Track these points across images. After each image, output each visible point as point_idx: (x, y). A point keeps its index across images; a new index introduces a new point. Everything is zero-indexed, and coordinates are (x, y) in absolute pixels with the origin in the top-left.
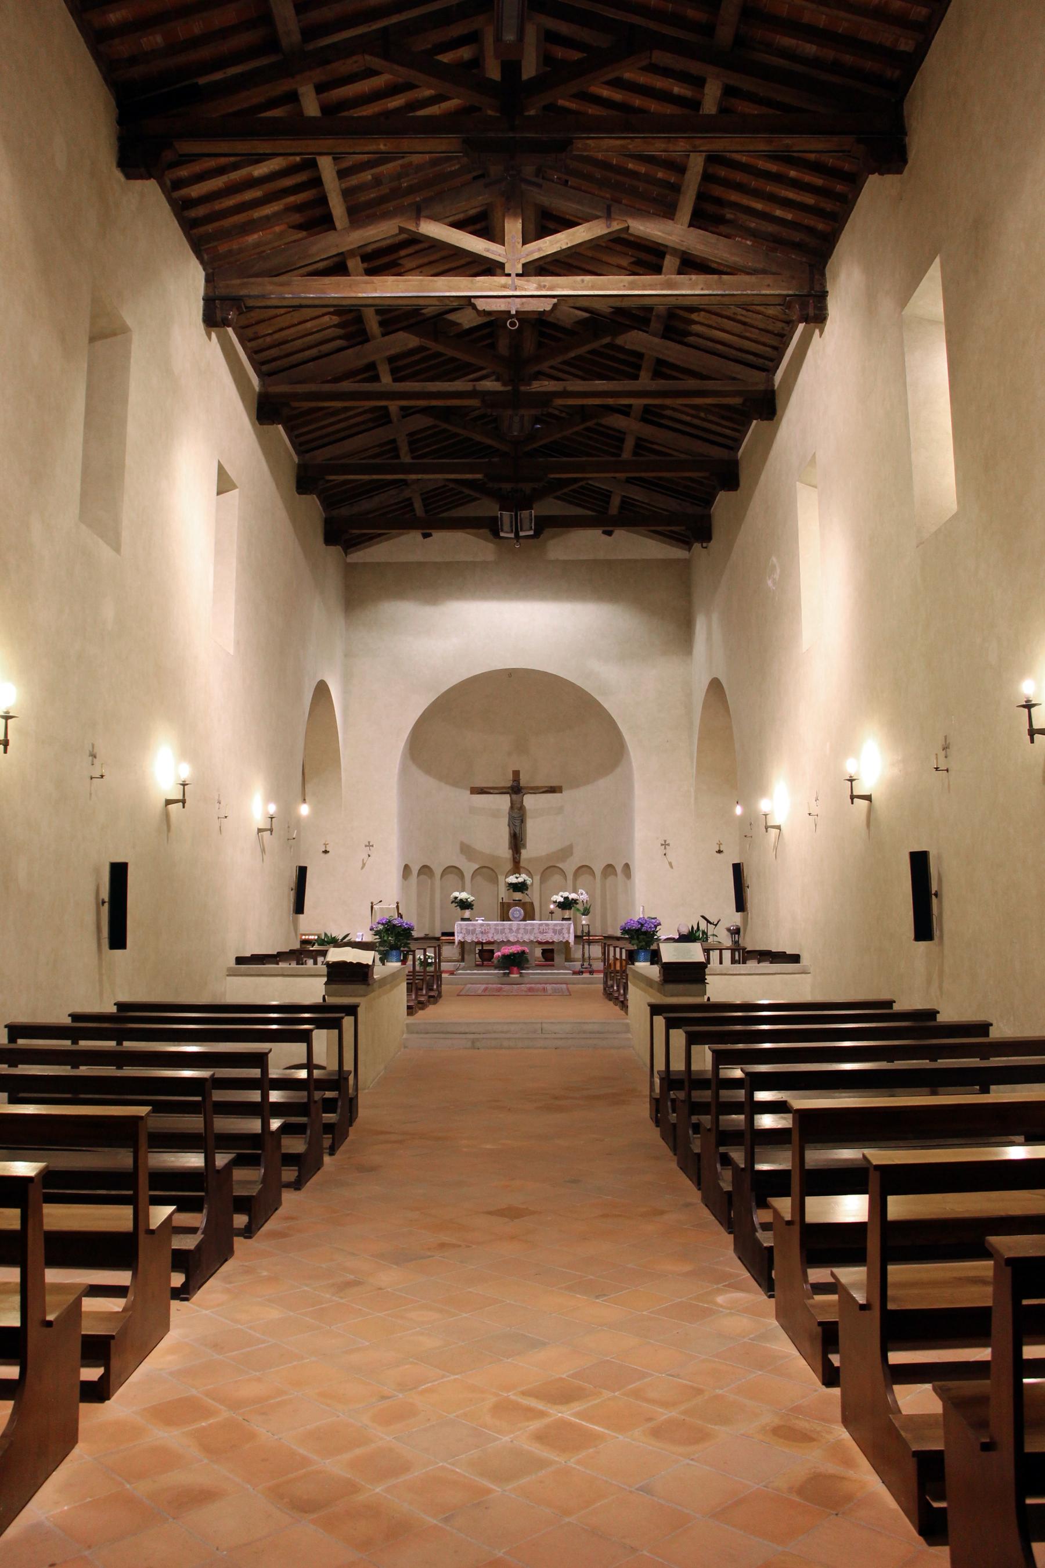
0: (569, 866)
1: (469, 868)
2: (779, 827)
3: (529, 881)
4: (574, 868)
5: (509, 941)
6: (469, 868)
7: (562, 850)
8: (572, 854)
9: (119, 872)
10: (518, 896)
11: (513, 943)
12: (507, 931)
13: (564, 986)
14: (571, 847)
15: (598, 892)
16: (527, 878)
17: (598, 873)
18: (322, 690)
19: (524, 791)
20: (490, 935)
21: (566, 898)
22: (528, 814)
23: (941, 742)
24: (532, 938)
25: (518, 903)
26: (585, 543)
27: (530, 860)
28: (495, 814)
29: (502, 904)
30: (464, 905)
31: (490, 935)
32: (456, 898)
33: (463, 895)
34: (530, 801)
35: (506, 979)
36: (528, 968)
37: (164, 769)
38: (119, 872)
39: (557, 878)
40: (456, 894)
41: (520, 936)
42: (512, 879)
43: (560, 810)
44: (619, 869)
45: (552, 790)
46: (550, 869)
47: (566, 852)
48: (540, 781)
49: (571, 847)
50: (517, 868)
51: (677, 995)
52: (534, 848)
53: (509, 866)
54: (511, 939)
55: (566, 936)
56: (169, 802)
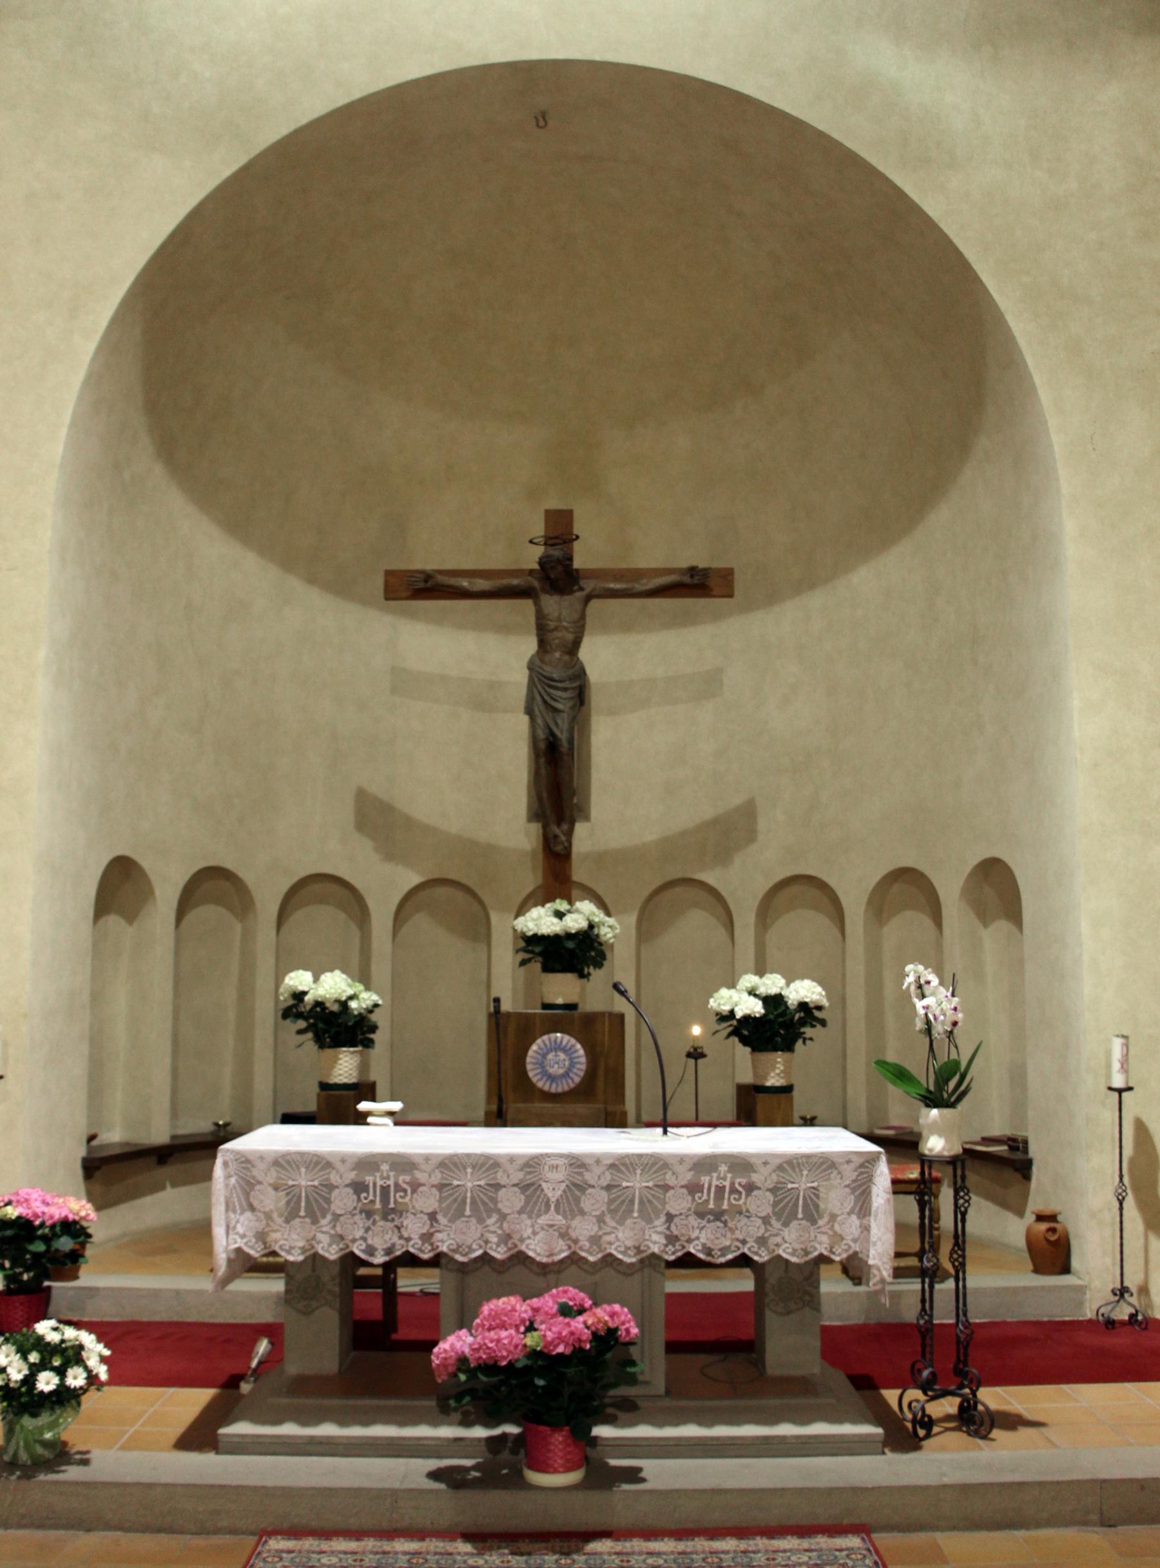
0: (744, 880)
1: (385, 882)
3: (609, 929)
4: (763, 885)
5: (520, 1259)
6: (385, 882)
7: (715, 822)
8: (751, 836)
10: (561, 988)
11: (547, 1273)
12: (510, 1200)
13: (854, 1541)
14: (748, 813)
15: (856, 969)
16: (599, 916)
17: (854, 903)
19: (589, 585)
20: (414, 1227)
21: (773, 1002)
22: (596, 699)
24: (656, 1243)
25: (564, 1017)
27: (601, 859)
28: (481, 699)
29: (497, 1017)
30: (336, 1027)
31: (414, 1227)
32: (299, 996)
33: (332, 986)
34: (608, 655)
35: (494, 1507)
36: (629, 1410)
39: (695, 926)
40: (299, 979)
41: (583, 1229)
42: (541, 921)
43: (708, 685)
44: (950, 888)
45: (698, 585)
46: (674, 890)
47: (733, 830)
48: (660, 551)
49: (748, 813)
50: (557, 877)
51: (1043, 1288)
52: (622, 810)
53: (530, 879)
54: (537, 1248)
55: (851, 1227)
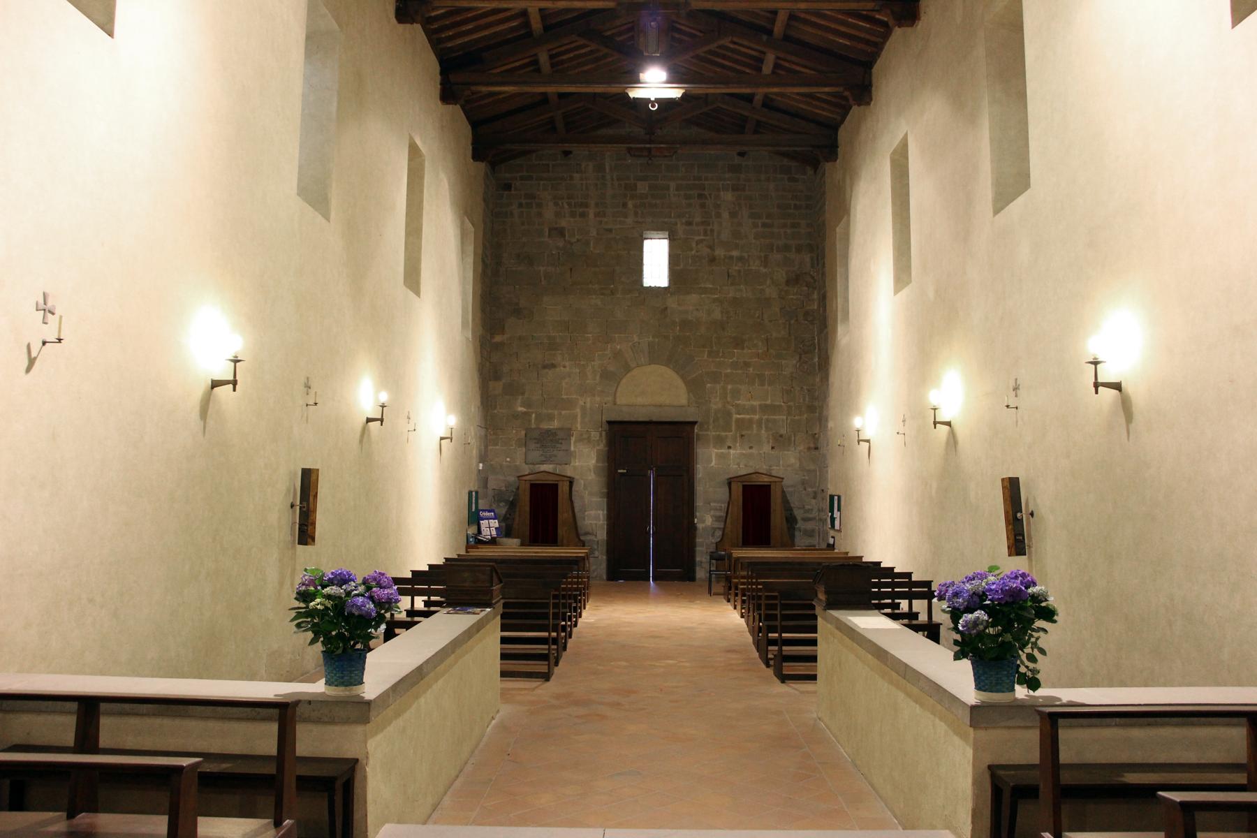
2: (868, 441)
9: (308, 479)
18: (904, 145)
23: (1012, 384)
26: (848, 181)
37: (365, 395)
38: (308, 479)
56: (369, 420)
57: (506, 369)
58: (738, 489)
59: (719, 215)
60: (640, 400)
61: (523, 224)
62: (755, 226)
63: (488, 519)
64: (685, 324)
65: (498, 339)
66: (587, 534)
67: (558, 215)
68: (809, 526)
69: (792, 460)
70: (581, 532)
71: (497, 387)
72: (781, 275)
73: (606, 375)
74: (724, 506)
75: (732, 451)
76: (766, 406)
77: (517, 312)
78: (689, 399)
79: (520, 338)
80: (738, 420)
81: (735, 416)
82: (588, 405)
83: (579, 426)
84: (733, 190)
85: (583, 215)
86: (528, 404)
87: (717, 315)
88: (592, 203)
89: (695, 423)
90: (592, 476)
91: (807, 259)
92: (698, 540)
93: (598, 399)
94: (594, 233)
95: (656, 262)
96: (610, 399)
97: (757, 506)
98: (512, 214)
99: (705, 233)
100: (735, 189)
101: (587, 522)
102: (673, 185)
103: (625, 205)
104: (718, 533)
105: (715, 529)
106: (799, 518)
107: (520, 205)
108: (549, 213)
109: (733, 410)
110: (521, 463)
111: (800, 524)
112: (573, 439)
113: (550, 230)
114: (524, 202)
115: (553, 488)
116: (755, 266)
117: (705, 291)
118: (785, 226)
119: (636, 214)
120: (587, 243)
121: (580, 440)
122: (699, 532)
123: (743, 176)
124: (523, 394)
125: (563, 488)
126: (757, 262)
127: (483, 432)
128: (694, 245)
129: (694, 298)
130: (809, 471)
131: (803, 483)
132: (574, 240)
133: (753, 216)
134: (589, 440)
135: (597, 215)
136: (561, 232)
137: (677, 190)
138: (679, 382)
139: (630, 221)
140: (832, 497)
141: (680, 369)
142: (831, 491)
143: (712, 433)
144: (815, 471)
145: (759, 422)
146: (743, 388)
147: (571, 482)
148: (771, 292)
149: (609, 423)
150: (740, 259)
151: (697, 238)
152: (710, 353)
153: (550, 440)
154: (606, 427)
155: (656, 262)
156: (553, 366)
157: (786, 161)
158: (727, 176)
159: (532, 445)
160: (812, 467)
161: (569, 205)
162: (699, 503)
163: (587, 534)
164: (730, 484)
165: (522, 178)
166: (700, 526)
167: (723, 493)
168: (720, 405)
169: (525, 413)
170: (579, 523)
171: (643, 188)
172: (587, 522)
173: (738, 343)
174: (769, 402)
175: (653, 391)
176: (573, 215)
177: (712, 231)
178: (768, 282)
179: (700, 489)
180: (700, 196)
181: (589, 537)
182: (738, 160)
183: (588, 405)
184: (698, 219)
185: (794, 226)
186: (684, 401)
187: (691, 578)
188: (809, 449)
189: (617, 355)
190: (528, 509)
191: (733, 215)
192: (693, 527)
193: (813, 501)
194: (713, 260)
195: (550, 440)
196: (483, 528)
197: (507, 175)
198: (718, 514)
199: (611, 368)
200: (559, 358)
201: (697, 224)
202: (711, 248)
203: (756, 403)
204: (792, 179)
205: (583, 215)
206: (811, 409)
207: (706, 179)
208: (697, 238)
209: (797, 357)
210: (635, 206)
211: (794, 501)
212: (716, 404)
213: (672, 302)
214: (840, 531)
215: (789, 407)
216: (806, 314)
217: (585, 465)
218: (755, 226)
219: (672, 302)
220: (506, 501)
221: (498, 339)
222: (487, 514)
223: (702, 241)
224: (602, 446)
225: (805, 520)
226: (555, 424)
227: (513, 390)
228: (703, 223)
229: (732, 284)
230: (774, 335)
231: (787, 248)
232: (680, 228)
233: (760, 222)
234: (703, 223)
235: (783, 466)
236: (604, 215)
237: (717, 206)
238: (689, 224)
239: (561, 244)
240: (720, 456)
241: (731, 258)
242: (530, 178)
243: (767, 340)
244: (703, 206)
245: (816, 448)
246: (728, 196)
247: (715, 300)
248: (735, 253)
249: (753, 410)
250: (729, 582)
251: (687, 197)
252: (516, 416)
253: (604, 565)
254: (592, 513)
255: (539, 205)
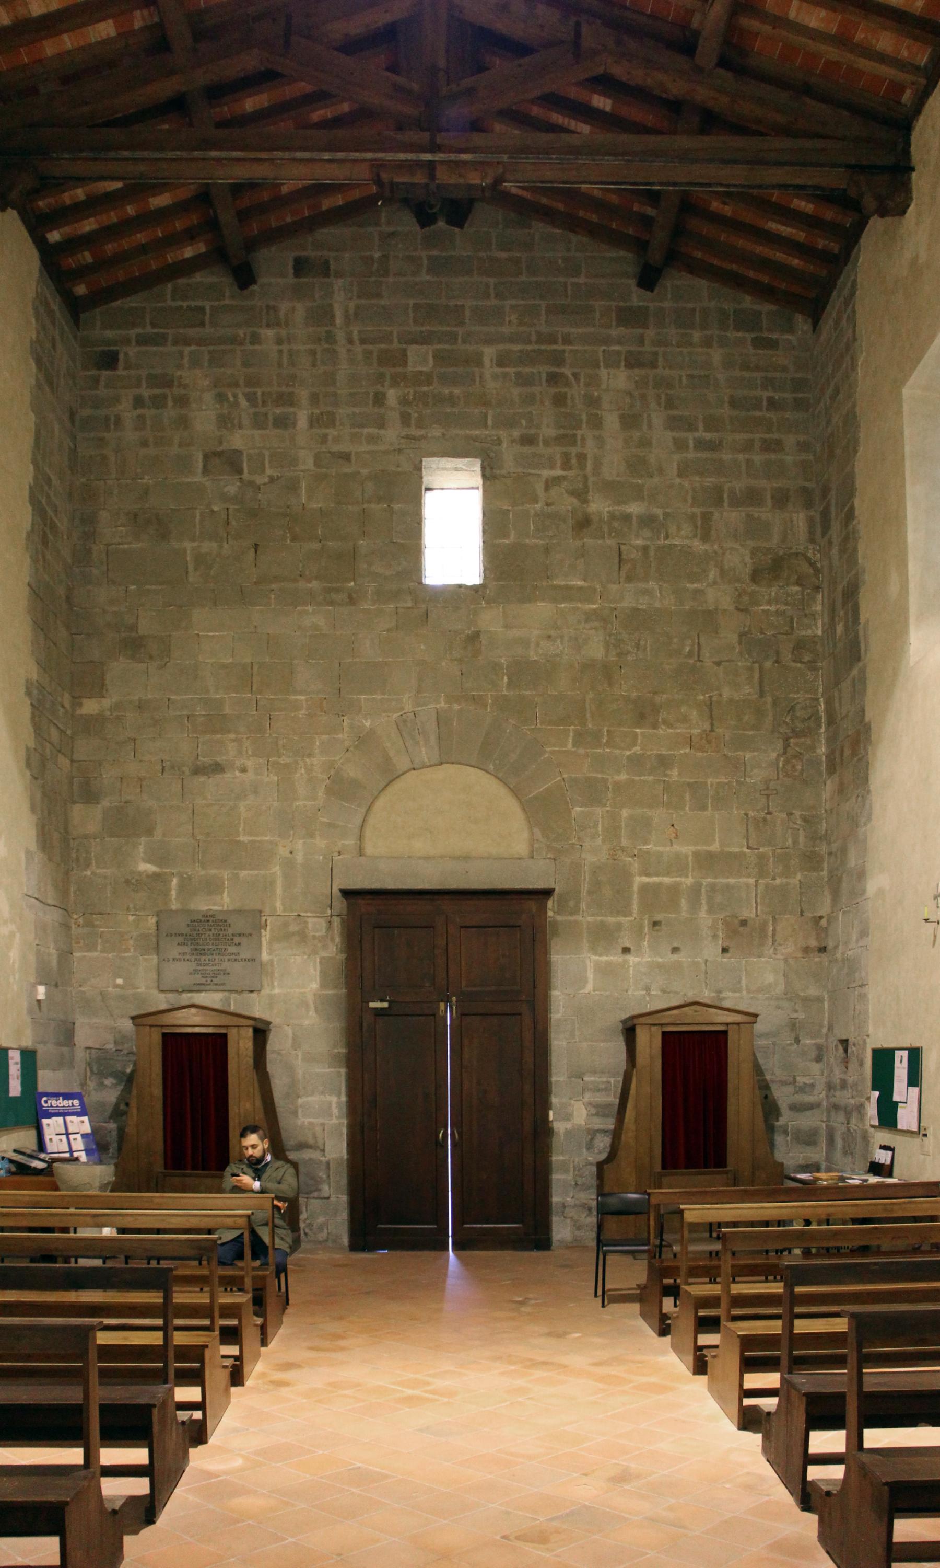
57: (108, 775)
58: (649, 1044)
59: (596, 422)
60: (420, 846)
61: (145, 444)
62: (680, 445)
63: (64, 1114)
64: (523, 671)
65: (90, 707)
66: (302, 1146)
67: (224, 421)
68: (807, 1121)
69: (770, 978)
70: (289, 1139)
71: (87, 819)
72: (739, 558)
73: (341, 789)
74: (616, 1081)
75: (632, 959)
76: (711, 855)
77: (134, 645)
78: (532, 841)
79: (141, 706)
80: (644, 888)
81: (639, 880)
82: (300, 858)
83: (278, 904)
84: (629, 366)
85: (283, 423)
86: (161, 856)
87: (596, 650)
88: (303, 394)
89: (547, 893)
90: (311, 1019)
91: (800, 519)
92: (556, 1158)
93: (320, 843)
94: (307, 462)
95: (453, 528)
96: (351, 842)
97: (694, 1082)
98: (118, 421)
99: (566, 465)
100: (633, 361)
101: (303, 1120)
102: (489, 352)
103: (379, 399)
104: (603, 1143)
105: (593, 1133)
106: (783, 1104)
107: (138, 402)
108: (204, 417)
109: (635, 866)
110: (138, 985)
111: (786, 1119)
112: (266, 935)
113: (206, 457)
114: (146, 393)
115: (213, 1046)
116: (682, 537)
117: (568, 593)
118: (748, 447)
119: (405, 419)
120: (293, 487)
121: (284, 936)
122: (559, 1141)
123: (650, 333)
124: (150, 832)
125: (241, 1046)
126: (687, 529)
127: (53, 916)
128: (540, 488)
129: (543, 609)
130: (806, 1000)
131: (793, 1025)
132: (260, 480)
133: (673, 423)
134: (302, 936)
135: (314, 422)
136: (233, 462)
137: (501, 362)
138: (509, 803)
139: (392, 434)
140: (883, 1060)
141: (513, 776)
142: (880, 1038)
143: (587, 918)
144: (820, 1000)
145: (696, 890)
146: (658, 815)
147: (261, 1032)
148: (719, 597)
149: (347, 894)
150: (648, 521)
151: (546, 473)
152: (579, 738)
153: (210, 937)
154: (340, 904)
155: (453, 528)
156: (218, 768)
157: (748, 302)
158: (614, 332)
159: (174, 951)
160: (812, 991)
161: (251, 398)
162: (558, 1076)
163: (302, 1146)
164: (629, 1031)
165: (143, 341)
166: (560, 1126)
167: (614, 1052)
168: (604, 856)
169: (156, 876)
170: (285, 1120)
171: (420, 359)
172: (303, 1120)
173: (645, 713)
174: (715, 847)
175: (450, 826)
176: (259, 422)
177: (582, 457)
178: (713, 574)
179: (560, 1043)
180: (553, 379)
181: (307, 1155)
182: (638, 298)
183: (300, 858)
184: (548, 431)
185: (768, 446)
186: (520, 847)
187: (537, 1237)
188: (806, 950)
189: (364, 741)
190: (158, 1091)
191: (629, 421)
192: (542, 1132)
193: (816, 1068)
194: (583, 523)
195: (210, 937)
196: (48, 1134)
197: (109, 334)
198: (601, 1098)
199: (352, 771)
200: (232, 748)
201: (546, 443)
202: (581, 495)
203: (686, 849)
204: (759, 343)
205: (283, 423)
206: (812, 861)
207: (567, 340)
208: (546, 473)
209: (780, 745)
210: (404, 401)
211: (774, 1070)
212: (593, 853)
213: (490, 620)
214: (920, 1132)
215: (761, 857)
216: (800, 646)
217: (294, 993)
218: (680, 445)
219: (490, 620)
220: (117, 1075)
221: (90, 707)
222: (62, 1103)
223: (557, 480)
224: (333, 949)
225: (796, 1108)
226: (225, 902)
227: (126, 824)
228: (560, 440)
229: (629, 579)
230: (726, 693)
231: (752, 497)
232: (509, 454)
233: (690, 437)
234: (560, 440)
235: (750, 987)
236: (332, 423)
237: (593, 402)
238: (527, 440)
239: (232, 489)
240: (605, 971)
241: (627, 518)
242: (159, 340)
243: (710, 705)
244: (559, 400)
245: (823, 950)
246: (618, 380)
247: (589, 617)
248: (635, 508)
249: (678, 866)
250: (668, 1281)
251: (524, 381)
252: (135, 883)
253: (343, 1216)
254: (315, 1102)
255: (182, 401)
